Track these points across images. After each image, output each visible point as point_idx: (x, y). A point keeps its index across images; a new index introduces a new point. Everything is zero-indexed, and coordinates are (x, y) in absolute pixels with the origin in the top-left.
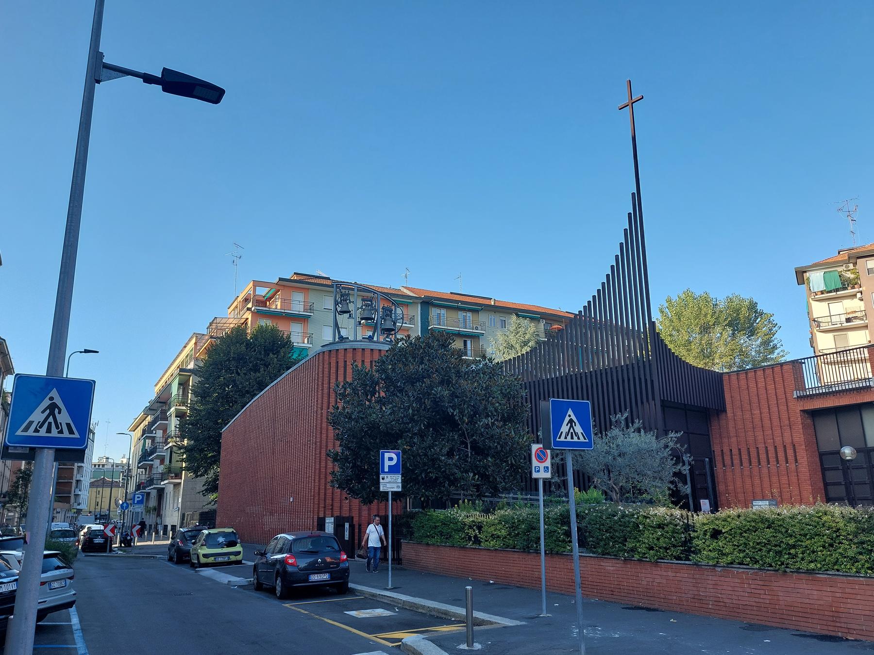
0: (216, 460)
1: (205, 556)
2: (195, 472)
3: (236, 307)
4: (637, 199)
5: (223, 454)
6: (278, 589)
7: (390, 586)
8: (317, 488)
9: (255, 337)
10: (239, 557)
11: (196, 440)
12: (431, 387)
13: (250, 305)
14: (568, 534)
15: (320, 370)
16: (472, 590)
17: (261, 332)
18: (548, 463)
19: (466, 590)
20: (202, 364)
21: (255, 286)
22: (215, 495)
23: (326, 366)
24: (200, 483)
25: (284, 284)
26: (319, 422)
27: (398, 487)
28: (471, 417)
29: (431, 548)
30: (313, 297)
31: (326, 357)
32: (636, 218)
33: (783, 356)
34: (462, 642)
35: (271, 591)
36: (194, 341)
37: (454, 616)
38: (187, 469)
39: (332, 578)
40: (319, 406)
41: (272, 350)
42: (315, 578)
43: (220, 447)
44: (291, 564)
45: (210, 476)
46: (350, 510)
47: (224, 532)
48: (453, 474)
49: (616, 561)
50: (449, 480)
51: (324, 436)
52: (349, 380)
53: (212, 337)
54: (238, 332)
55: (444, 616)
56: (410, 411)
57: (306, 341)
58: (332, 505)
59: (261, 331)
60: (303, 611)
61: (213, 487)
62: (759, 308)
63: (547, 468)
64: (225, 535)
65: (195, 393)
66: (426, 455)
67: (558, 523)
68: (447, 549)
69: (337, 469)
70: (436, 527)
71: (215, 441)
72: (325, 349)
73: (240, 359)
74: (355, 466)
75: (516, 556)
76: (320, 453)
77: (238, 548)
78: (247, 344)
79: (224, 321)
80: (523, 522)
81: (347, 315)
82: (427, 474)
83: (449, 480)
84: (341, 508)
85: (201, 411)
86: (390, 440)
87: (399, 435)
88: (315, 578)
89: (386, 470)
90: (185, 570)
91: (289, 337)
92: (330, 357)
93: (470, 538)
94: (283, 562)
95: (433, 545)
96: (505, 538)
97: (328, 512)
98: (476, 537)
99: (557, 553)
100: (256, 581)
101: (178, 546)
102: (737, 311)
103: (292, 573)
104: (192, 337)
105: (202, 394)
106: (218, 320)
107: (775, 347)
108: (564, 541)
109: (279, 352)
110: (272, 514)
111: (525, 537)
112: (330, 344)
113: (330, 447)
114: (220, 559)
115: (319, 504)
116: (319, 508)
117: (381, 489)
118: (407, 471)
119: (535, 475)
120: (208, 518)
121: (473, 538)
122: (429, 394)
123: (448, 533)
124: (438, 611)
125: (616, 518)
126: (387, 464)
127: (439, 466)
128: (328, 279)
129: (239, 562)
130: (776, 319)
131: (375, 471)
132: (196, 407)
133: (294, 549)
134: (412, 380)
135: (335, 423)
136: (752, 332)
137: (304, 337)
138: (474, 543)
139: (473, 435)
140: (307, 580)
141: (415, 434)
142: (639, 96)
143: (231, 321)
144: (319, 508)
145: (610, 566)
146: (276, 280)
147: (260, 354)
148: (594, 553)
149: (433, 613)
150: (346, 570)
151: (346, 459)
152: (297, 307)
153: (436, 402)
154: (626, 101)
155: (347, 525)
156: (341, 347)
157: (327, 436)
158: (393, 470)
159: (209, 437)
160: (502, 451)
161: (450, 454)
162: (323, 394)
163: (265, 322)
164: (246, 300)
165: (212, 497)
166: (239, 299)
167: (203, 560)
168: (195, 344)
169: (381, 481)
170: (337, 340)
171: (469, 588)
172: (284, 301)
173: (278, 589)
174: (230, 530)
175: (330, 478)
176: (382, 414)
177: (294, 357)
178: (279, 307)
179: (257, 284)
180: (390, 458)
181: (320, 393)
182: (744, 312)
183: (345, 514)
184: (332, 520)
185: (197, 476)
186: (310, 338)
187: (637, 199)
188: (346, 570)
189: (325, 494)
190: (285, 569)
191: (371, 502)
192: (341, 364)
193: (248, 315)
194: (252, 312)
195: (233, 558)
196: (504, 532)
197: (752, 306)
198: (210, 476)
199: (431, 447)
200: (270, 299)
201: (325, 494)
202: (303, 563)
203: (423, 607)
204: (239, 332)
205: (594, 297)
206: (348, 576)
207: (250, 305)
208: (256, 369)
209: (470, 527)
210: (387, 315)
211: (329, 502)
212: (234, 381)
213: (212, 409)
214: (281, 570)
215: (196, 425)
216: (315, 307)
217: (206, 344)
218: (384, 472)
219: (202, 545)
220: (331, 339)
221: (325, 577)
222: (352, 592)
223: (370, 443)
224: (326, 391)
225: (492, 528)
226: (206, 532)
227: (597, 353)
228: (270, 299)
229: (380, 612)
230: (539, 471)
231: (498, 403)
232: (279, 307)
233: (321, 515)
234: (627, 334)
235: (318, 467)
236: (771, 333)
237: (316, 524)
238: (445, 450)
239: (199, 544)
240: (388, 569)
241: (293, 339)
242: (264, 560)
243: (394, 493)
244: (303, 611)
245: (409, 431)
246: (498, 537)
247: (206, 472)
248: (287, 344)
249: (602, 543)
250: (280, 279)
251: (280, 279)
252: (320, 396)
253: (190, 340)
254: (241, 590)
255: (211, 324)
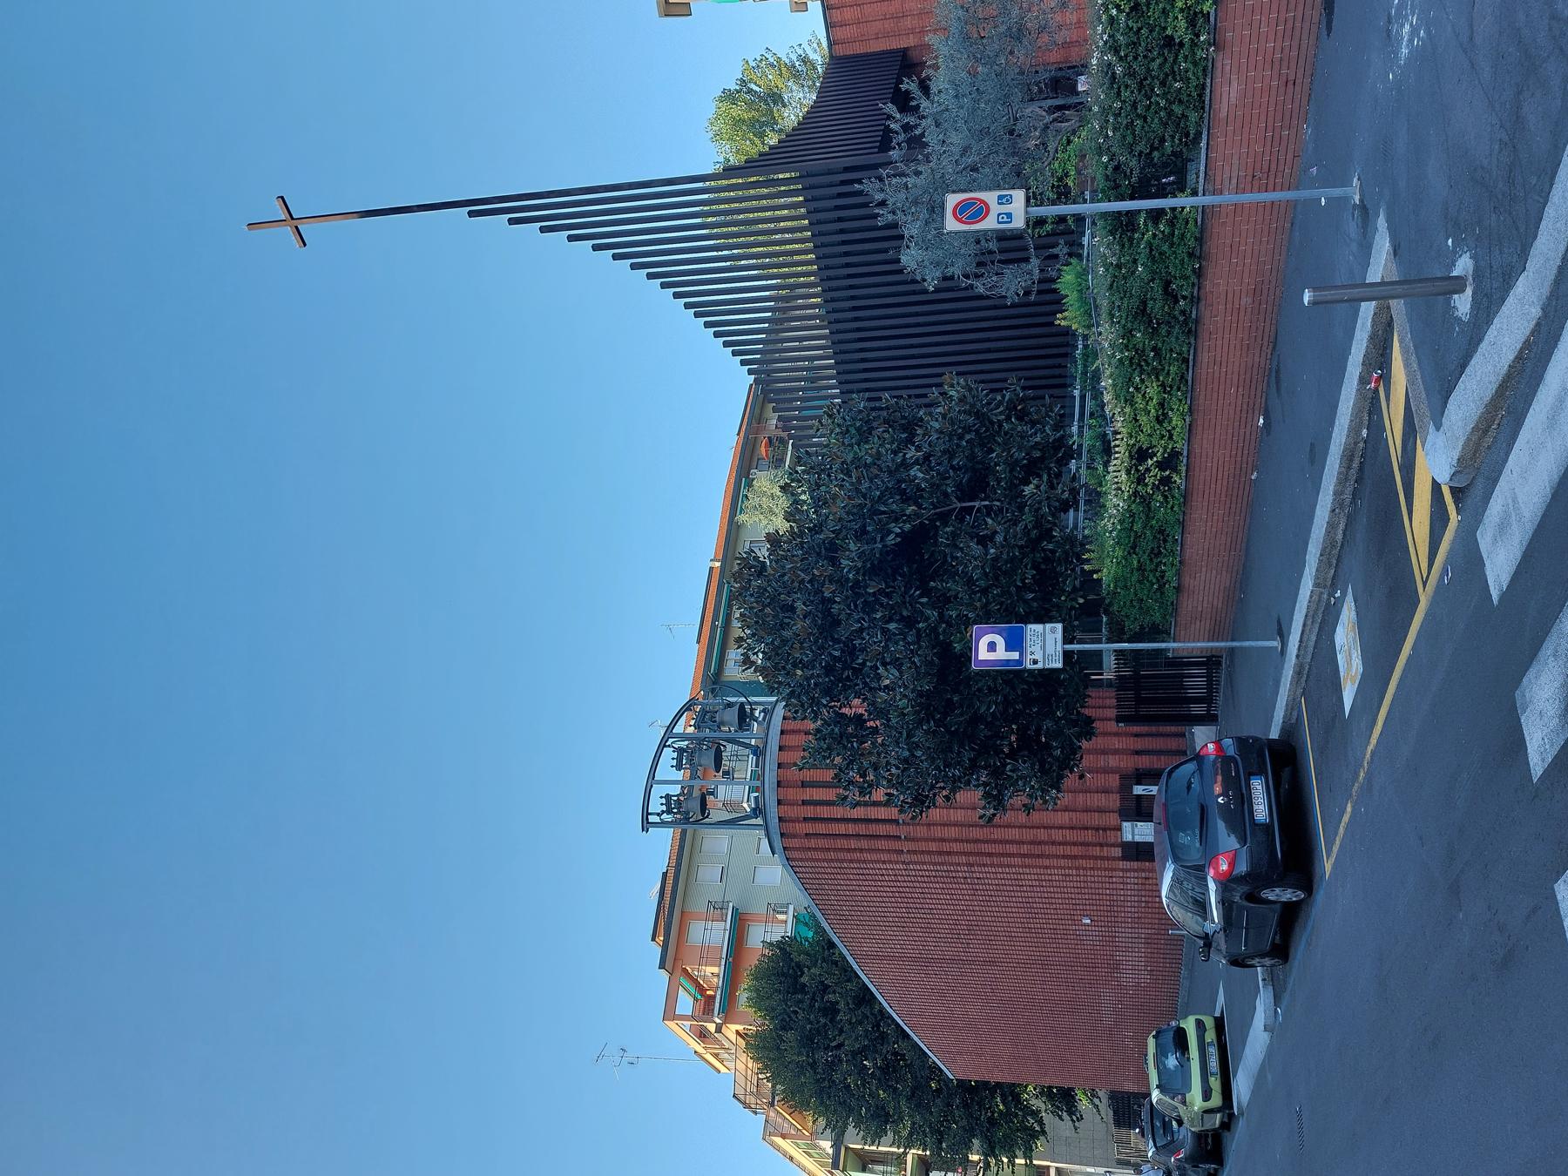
0: (1012, 1092)
1: (1207, 1095)
2: (1033, 1135)
3: (716, 1056)
4: (480, 207)
5: (995, 1077)
6: (1289, 895)
7: (1276, 644)
8: (1062, 862)
9: (769, 1011)
10: (1209, 1022)
11: (971, 1133)
12: (841, 582)
13: (712, 1027)
14: (1156, 215)
15: (821, 855)
16: (1315, 289)
17: (760, 1001)
18: (990, 197)
19: (1314, 303)
20: (822, 1122)
21: (675, 1017)
22: (1080, 1095)
23: (813, 843)
24: (1060, 1127)
25: (672, 958)
26: (927, 858)
27: (1053, 631)
28: (906, 499)
29: (1186, 580)
30: (699, 905)
31: (795, 843)
32: (520, 208)
33: (819, 44)
34: (1449, 308)
35: (1290, 916)
36: (778, 1140)
37: (1358, 432)
38: (1028, 1155)
39: (1261, 772)
40: (894, 857)
41: (796, 978)
42: (1261, 811)
43: (986, 1084)
44: (1232, 865)
45: (1043, 1107)
46: (1106, 791)
47: (1156, 1056)
48: (1026, 532)
49: (1218, 73)
50: (1040, 539)
51: (956, 847)
52: (829, 775)
53: (772, 1104)
54: (757, 1048)
55: (1355, 465)
56: (892, 626)
57: (781, 917)
58: (1097, 829)
59: (758, 1001)
60: (1346, 818)
61: (1064, 1099)
62: (734, 87)
63: (1000, 197)
64: (1161, 1053)
65: (876, 1137)
66: (985, 591)
67: (1131, 239)
68: (1189, 539)
69: (1019, 800)
70: (1141, 568)
71: (973, 1093)
72: (778, 845)
73: (808, 1041)
74: (1013, 755)
75: (1204, 357)
76: (990, 855)
77: (1189, 1025)
78: (783, 1028)
79: (741, 1080)
80: (1128, 334)
81: (710, 798)
82: (1025, 588)
83: (1040, 539)
84: (1100, 811)
85: (913, 1123)
86: (954, 660)
87: (945, 649)
88: (1261, 811)
89: (1015, 655)
90: (1237, 1144)
91: (771, 944)
92: (794, 836)
93: (1166, 481)
94: (1226, 883)
95: (1178, 573)
96: (1163, 385)
97: (1111, 837)
98: (1161, 466)
99: (1200, 240)
100: (1268, 962)
101: (1188, 1159)
102: (737, 122)
103: (1253, 862)
104: (772, 1144)
105: (879, 1121)
106: (740, 1091)
107: (805, 60)
108: (1171, 223)
109: (798, 965)
110: (1116, 967)
111: (1164, 330)
112: (768, 835)
113: (974, 816)
114: (1214, 1063)
115: (1096, 858)
116: (1102, 858)
117: (1059, 665)
118: (1014, 614)
119: (1019, 223)
120: (1128, 1109)
121: (1160, 468)
122: (857, 582)
123: (1153, 539)
124: (1342, 480)
125: (1119, 70)
126: (1001, 653)
127: (1012, 560)
128: (665, 875)
129: (1219, 1024)
130: (753, 55)
131: (1017, 683)
132: (905, 1133)
133: (1195, 857)
134: (828, 624)
135: (921, 801)
136: (775, 98)
137: (775, 920)
138: (1175, 470)
139: (946, 495)
140: (1267, 828)
141: (941, 615)
142: (278, 204)
143: (741, 1066)
144: (1102, 858)
145: (1228, 93)
146: (664, 975)
147: (801, 1001)
148: (1199, 134)
149: (1347, 497)
150: (1242, 742)
151: (996, 773)
152: (717, 933)
153: (875, 569)
154: (288, 230)
155: (1138, 790)
156: (773, 811)
157: (956, 840)
158: (1015, 642)
159: (966, 1106)
160: (977, 431)
161: (983, 541)
162: (869, 850)
163: (743, 996)
164: (702, 1035)
165: (1084, 1104)
166: (700, 1049)
167: (1216, 1100)
168: (784, 1137)
169: (1040, 666)
170: (759, 821)
171: (1307, 297)
172: (704, 960)
173: (1289, 895)
174: (1151, 1042)
175: (1036, 817)
176: (897, 684)
177: (810, 934)
178: (715, 970)
179: (670, 1014)
180: (990, 648)
181: (867, 856)
182: (736, 111)
183: (1114, 801)
184: (1127, 825)
185: (1043, 1132)
186: (765, 888)
187: (480, 207)
188: (1242, 742)
189: (1075, 844)
190: (1241, 879)
191: (1089, 721)
192: (809, 811)
193: (731, 1030)
194: (725, 1022)
195: (1210, 1036)
196: (1152, 390)
197: (729, 97)
198: (1043, 1107)
199: (970, 582)
200: (701, 990)
201: (1075, 844)
202: (1228, 841)
203: (1331, 526)
204: (764, 1048)
205: (677, 296)
206: (1256, 739)
207: (712, 1027)
208: (831, 1010)
209: (1140, 480)
210: (712, 719)
211: (1089, 836)
212: (854, 1054)
213: (909, 1099)
214: (1246, 888)
215: (941, 1133)
216: (717, 898)
217: (782, 1115)
218: (1019, 662)
219: (1184, 1103)
220: (761, 833)
221: (1258, 787)
222: (1291, 730)
223: (962, 715)
224: (864, 844)
225: (1143, 419)
226: (1155, 1095)
227: (813, 380)
228: (701, 990)
229: (1345, 636)
230: (1009, 215)
231: (880, 445)
232: (715, 970)
233: (1118, 852)
234: (782, 321)
235: (1018, 861)
236: (778, 65)
237: (1135, 865)
238: (976, 549)
239: (1182, 1109)
240: (1232, 650)
241: (776, 938)
242: (1221, 940)
243: (1067, 639)
244: (1346, 818)
245: (934, 630)
246: (1161, 404)
247: (1035, 1114)
248: (783, 948)
249: (1178, 109)
250: (662, 966)
251: (662, 966)
252: (875, 857)
253: (778, 1148)
254: (1285, 1002)
255: (747, 1106)
